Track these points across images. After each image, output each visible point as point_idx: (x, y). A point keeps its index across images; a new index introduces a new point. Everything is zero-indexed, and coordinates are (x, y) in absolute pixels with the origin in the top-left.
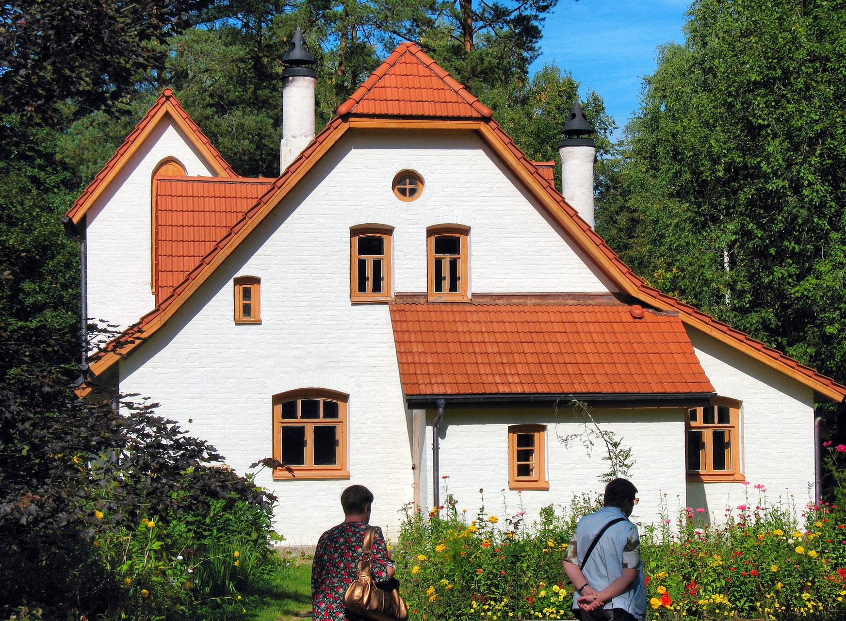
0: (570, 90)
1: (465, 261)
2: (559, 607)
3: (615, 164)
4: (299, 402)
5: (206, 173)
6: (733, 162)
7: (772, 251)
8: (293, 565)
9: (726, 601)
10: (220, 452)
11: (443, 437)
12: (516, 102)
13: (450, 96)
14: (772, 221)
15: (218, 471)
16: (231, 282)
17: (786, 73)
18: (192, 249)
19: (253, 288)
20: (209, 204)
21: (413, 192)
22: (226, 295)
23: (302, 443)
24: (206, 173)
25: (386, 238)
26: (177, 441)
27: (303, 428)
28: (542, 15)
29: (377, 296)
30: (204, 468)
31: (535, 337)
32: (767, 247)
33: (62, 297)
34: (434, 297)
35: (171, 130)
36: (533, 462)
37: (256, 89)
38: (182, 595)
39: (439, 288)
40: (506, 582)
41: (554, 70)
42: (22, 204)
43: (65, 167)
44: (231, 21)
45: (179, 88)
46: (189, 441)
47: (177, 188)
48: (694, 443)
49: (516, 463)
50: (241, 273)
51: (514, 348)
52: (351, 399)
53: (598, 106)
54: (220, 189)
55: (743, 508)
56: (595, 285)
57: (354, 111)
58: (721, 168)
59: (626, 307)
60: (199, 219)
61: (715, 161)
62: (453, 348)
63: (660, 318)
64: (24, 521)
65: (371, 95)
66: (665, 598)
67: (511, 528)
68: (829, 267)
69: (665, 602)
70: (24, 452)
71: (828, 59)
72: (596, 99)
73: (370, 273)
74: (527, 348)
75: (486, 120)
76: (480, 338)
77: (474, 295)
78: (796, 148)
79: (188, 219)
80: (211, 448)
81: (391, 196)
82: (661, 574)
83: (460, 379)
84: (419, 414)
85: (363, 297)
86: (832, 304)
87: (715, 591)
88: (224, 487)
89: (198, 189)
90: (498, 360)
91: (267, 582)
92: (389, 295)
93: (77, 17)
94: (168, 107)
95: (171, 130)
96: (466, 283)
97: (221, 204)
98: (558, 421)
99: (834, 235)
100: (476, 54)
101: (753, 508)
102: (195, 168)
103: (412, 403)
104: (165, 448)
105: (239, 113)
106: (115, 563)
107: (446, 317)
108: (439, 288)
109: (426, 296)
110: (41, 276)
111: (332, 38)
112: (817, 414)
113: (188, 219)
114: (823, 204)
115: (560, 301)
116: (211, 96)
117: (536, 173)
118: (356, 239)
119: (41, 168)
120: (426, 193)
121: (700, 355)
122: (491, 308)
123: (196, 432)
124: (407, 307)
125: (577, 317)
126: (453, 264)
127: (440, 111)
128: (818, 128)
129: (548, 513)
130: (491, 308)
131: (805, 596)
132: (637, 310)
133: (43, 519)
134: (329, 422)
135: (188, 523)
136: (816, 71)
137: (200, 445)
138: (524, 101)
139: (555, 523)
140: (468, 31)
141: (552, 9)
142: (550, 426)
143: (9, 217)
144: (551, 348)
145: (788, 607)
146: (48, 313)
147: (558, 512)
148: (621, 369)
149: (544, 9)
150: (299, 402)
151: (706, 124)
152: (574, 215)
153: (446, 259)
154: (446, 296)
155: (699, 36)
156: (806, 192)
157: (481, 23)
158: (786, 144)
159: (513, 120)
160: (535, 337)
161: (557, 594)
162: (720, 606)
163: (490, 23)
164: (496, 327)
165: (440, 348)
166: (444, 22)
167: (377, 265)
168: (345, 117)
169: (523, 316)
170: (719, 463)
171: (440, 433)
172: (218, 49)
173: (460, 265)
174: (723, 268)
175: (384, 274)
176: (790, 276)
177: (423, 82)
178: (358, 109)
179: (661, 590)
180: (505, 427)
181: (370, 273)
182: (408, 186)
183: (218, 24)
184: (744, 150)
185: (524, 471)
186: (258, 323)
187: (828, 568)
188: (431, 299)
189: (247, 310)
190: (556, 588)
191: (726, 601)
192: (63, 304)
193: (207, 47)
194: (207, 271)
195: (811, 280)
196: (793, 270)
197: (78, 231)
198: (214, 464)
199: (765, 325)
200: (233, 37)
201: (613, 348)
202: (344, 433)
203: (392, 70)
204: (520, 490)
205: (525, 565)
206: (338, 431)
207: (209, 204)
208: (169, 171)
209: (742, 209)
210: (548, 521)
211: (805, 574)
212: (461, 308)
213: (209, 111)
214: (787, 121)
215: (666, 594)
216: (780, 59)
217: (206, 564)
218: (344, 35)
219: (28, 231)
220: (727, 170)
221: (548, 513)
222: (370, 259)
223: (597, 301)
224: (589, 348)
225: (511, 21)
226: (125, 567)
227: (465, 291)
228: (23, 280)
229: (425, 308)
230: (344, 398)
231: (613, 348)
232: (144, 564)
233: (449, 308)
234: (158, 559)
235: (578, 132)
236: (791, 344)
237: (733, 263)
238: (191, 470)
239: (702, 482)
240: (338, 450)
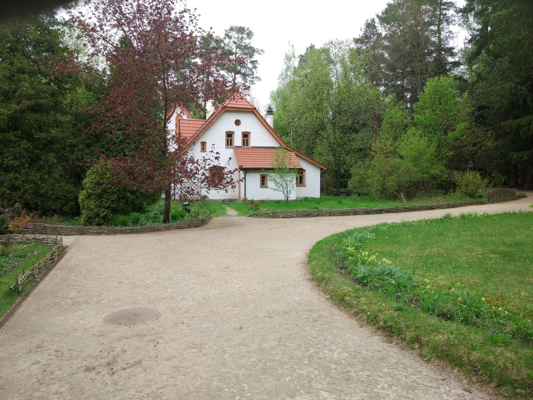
21: (239, 124)
77: (252, 147)
85: (228, 147)
152: (267, 124)
154: (246, 147)
167: (231, 140)
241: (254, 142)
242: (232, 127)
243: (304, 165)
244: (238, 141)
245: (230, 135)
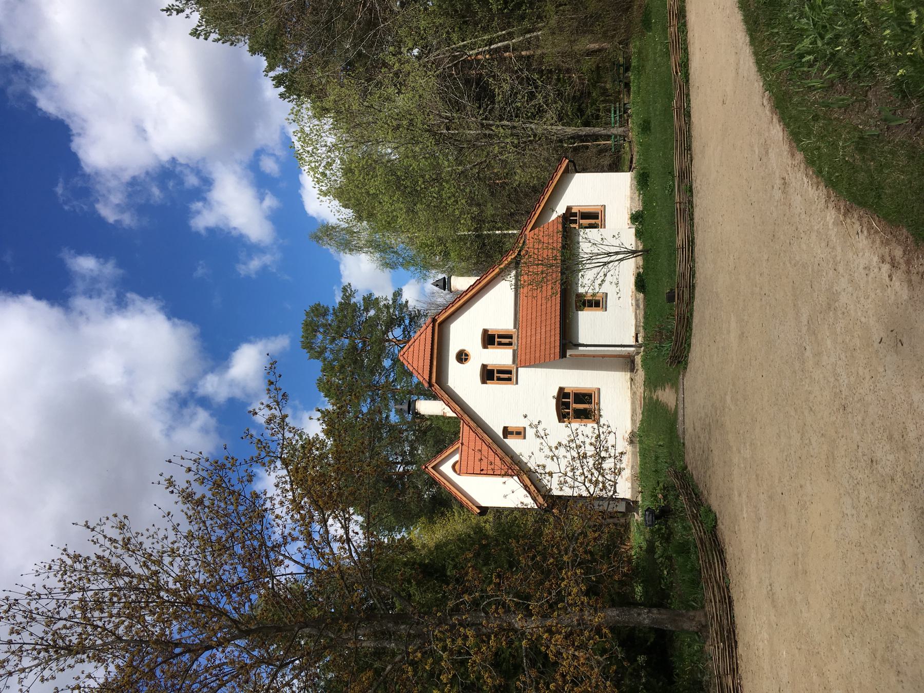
16: (505, 440)
21: (467, 355)
22: (513, 443)
65: (411, 362)
77: (515, 327)
95: (441, 468)
102: (456, 458)
108: (510, 344)
120: (469, 350)
132: (523, 253)
154: (514, 340)
168: (430, 385)
177: (416, 348)
178: (427, 378)
188: (516, 348)
189: (518, 433)
197: (484, 510)
233: (520, 339)
241: (504, 322)
242: (473, 369)
244: (501, 357)
245: (488, 375)
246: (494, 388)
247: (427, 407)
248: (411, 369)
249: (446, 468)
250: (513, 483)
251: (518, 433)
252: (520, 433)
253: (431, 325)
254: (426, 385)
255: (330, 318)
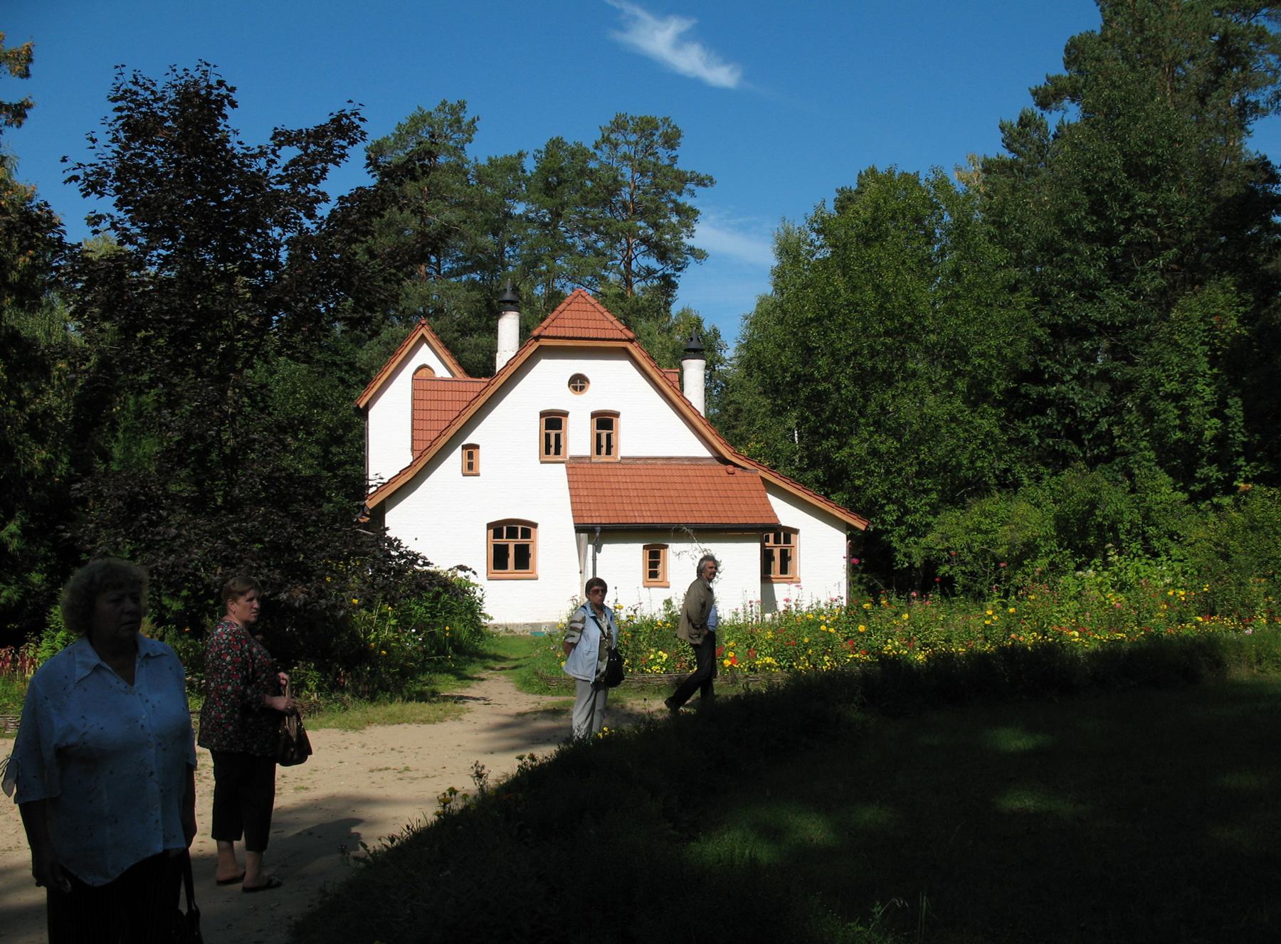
0: (698, 323)
1: (617, 435)
2: (663, 665)
3: (727, 372)
4: (505, 528)
5: (447, 375)
6: (796, 371)
7: (821, 430)
8: (497, 637)
9: (774, 662)
10: (430, 560)
11: (599, 552)
12: (663, 331)
13: (607, 325)
14: (823, 410)
15: (428, 573)
16: (460, 447)
17: (831, 314)
18: (435, 425)
19: (475, 451)
20: (448, 396)
21: (582, 388)
22: (457, 456)
23: (507, 555)
24: (447, 375)
25: (563, 419)
26: (401, 553)
27: (507, 546)
28: (678, 274)
29: (558, 458)
30: (418, 571)
31: (662, 486)
32: (818, 427)
33: (357, 457)
34: (596, 459)
35: (425, 346)
36: (660, 569)
37: (488, 320)
38: (414, 654)
39: (599, 452)
40: (628, 649)
41: (689, 310)
42: (332, 395)
43: (362, 371)
44: (473, 275)
45: (437, 319)
46: (409, 553)
47: (427, 385)
48: (767, 557)
49: (648, 570)
50: (467, 442)
51: (648, 493)
52: (539, 526)
53: (716, 334)
54: (456, 386)
55: (787, 600)
56: (704, 452)
57: (543, 334)
58: (788, 375)
59: (723, 467)
60: (442, 406)
61: (785, 370)
62: (607, 493)
63: (746, 474)
64: (297, 605)
65: (554, 324)
66: (733, 659)
67: (632, 613)
68: (858, 441)
69: (733, 662)
70: (301, 559)
71: (858, 305)
72: (715, 330)
73: (604, 442)
74: (657, 493)
75: (631, 341)
76: (625, 486)
78: (837, 362)
79: (434, 405)
80: (425, 558)
81: (568, 391)
82: (731, 644)
83: (611, 513)
84: (584, 536)
85: (549, 458)
86: (859, 466)
87: (766, 655)
88: (431, 584)
89: (441, 386)
90: (637, 501)
91: (476, 648)
92: (616, 458)
93: (335, 268)
94: (423, 331)
95: (425, 346)
96: (617, 449)
97: (457, 396)
98: (677, 542)
99: (862, 421)
100: (634, 298)
101: (794, 601)
102: (441, 372)
103: (579, 529)
104: (394, 557)
105: (475, 336)
106: (367, 633)
107: (602, 472)
108: (599, 452)
109: (590, 458)
110: (344, 443)
111: (539, 288)
112: (848, 538)
113: (434, 405)
114: (854, 400)
115: (680, 462)
116: (458, 325)
117: (664, 377)
118: (544, 419)
119: (346, 372)
121: (771, 498)
122: (633, 466)
123: (414, 548)
124: (577, 465)
125: (690, 473)
126: (609, 437)
127: (601, 334)
128: (851, 349)
129: (668, 603)
130: (633, 466)
131: (826, 658)
132: (730, 468)
133: (310, 603)
134: (525, 541)
135: (426, 607)
136: (850, 312)
137: (417, 556)
138: (669, 330)
139: (672, 610)
140: (629, 284)
141: (685, 270)
142: (670, 545)
143: (323, 404)
144: (672, 493)
145: (815, 666)
146: (348, 467)
147: (675, 603)
148: (719, 508)
149: (680, 269)
150: (505, 528)
151: (779, 346)
152: (689, 405)
153: (604, 433)
154: (603, 458)
155: (779, 289)
156: (843, 392)
157: (638, 279)
158: (830, 360)
159: (661, 343)
160: (662, 486)
161: (661, 657)
162: (770, 665)
163: (644, 279)
164: (636, 479)
165: (598, 493)
166: (613, 277)
167: (558, 437)
168: (537, 338)
169: (655, 473)
170: (784, 569)
171: (597, 549)
172: (463, 294)
173: (613, 437)
174: (794, 440)
175: (562, 443)
176: (832, 447)
177: (590, 315)
178: (546, 333)
179: (731, 654)
180: (641, 545)
181: (604, 442)
182: (579, 385)
183: (464, 278)
184: (805, 363)
185: (653, 575)
186: (478, 475)
187: (842, 640)
189: (470, 466)
190: (660, 652)
191: (774, 662)
192: (357, 461)
193: (455, 293)
194: (444, 440)
195: (847, 450)
196: (835, 443)
197: (363, 413)
198: (426, 568)
199: (817, 480)
200: (473, 285)
201: (714, 494)
202: (535, 548)
203: (569, 308)
204: (649, 587)
205: (641, 638)
206: (531, 547)
207: (448, 396)
208: (423, 373)
209: (802, 402)
210: (668, 608)
211: (827, 644)
212: (613, 466)
213: (456, 335)
214: (831, 344)
215: (734, 657)
216: (827, 304)
217: (432, 634)
218: (548, 285)
219: (335, 413)
220: (792, 377)
221: (668, 603)
222: (553, 433)
223: (705, 462)
224: (698, 493)
225: (658, 278)
226: (373, 637)
227: (616, 455)
228: (331, 445)
229: (589, 466)
230: (535, 525)
231: (714, 494)
232: (387, 633)
233: (605, 466)
234: (395, 632)
235: (695, 350)
236: (833, 492)
237: (800, 438)
238: (410, 572)
239: (772, 583)
240: (531, 560)
242: (562, 399)
243: (786, 514)
244: (579, 439)
245: (553, 421)
246: (533, 430)
247: (509, 326)
248: (560, 308)
249: (425, 355)
250: (404, 458)
251: (470, 466)
252: (470, 468)
253: (624, 337)
254: (535, 333)
255: (662, 153)
